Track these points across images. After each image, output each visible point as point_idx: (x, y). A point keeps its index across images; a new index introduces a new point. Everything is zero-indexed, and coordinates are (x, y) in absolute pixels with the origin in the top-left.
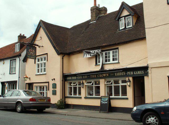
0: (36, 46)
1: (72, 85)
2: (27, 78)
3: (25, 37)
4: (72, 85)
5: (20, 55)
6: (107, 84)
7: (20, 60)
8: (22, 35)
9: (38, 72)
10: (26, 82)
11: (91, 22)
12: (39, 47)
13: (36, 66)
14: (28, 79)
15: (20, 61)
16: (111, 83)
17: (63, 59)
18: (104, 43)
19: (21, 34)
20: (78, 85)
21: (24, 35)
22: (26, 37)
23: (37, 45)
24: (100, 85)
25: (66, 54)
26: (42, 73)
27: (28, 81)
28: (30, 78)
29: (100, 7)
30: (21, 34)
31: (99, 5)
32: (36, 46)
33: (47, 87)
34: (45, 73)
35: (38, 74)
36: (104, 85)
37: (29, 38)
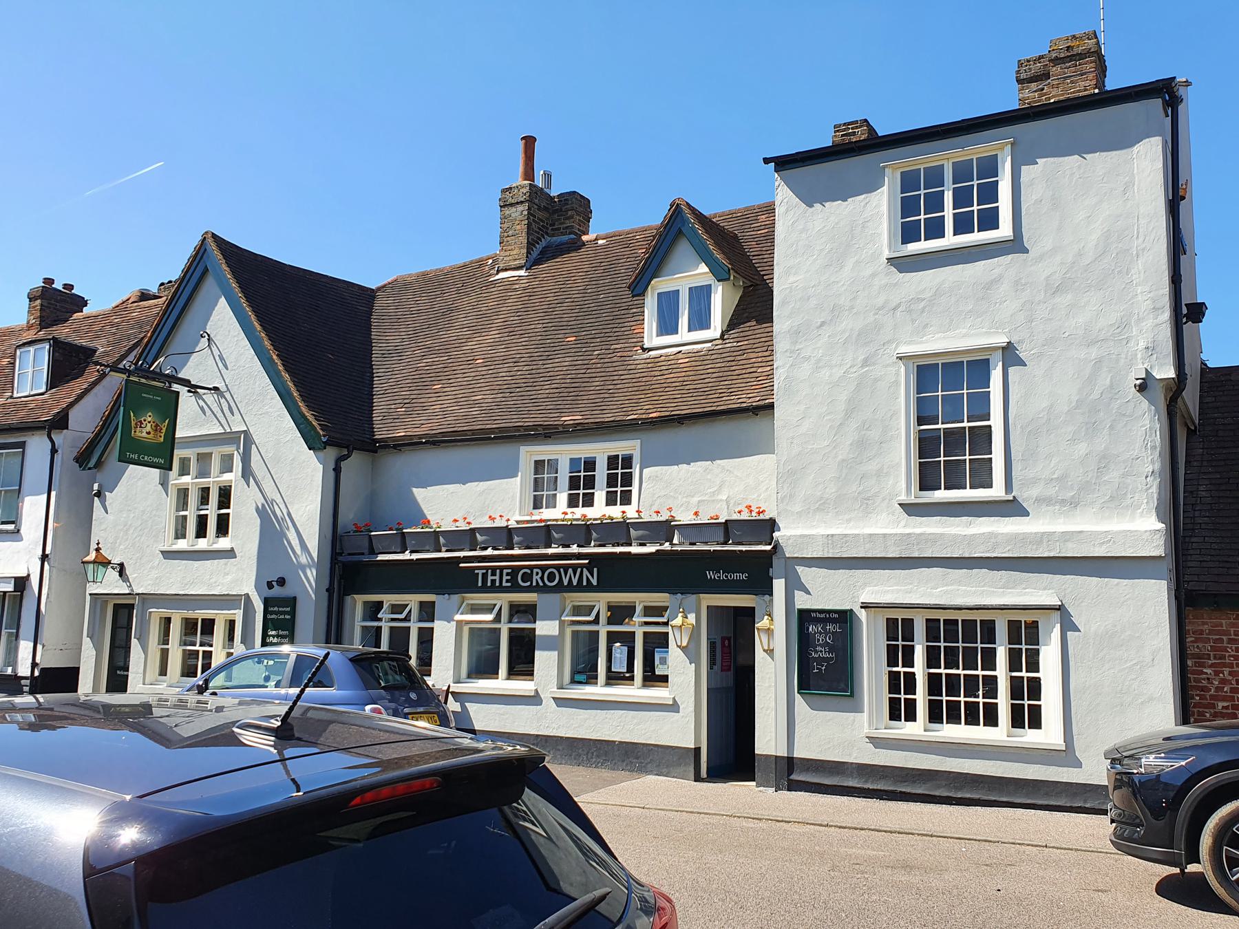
0: (176, 387)
1: (380, 620)
2: (106, 563)
3: (81, 303)
4: (380, 620)
5: (60, 422)
6: (574, 623)
7: (54, 451)
8: (58, 285)
9: (180, 534)
10: (93, 589)
11: (502, 275)
12: (193, 388)
13: (170, 502)
14: (112, 574)
15: (58, 457)
16: (402, 616)
17: (337, 470)
18: (572, 413)
19: (49, 281)
20: (603, 619)
21: (69, 287)
22: (84, 303)
23: (185, 382)
24: (970, 488)
25: (354, 449)
26: (202, 544)
27: (110, 584)
28: (122, 565)
29: (554, 193)
30: (49, 281)
31: (548, 176)
32: (176, 387)
33: (573, 621)
34: (224, 543)
35: (182, 545)
36: (604, 493)
37: (105, 316)
